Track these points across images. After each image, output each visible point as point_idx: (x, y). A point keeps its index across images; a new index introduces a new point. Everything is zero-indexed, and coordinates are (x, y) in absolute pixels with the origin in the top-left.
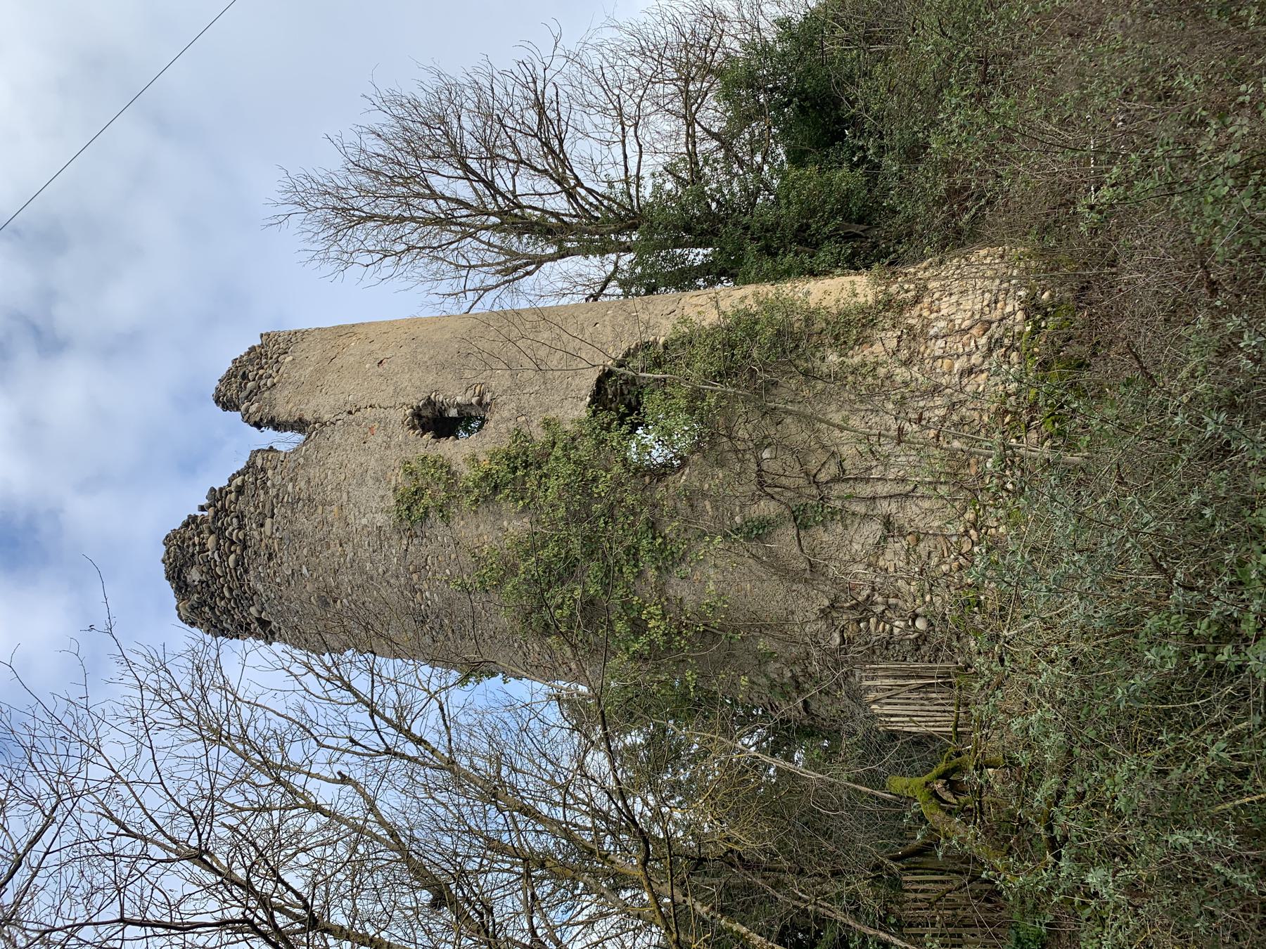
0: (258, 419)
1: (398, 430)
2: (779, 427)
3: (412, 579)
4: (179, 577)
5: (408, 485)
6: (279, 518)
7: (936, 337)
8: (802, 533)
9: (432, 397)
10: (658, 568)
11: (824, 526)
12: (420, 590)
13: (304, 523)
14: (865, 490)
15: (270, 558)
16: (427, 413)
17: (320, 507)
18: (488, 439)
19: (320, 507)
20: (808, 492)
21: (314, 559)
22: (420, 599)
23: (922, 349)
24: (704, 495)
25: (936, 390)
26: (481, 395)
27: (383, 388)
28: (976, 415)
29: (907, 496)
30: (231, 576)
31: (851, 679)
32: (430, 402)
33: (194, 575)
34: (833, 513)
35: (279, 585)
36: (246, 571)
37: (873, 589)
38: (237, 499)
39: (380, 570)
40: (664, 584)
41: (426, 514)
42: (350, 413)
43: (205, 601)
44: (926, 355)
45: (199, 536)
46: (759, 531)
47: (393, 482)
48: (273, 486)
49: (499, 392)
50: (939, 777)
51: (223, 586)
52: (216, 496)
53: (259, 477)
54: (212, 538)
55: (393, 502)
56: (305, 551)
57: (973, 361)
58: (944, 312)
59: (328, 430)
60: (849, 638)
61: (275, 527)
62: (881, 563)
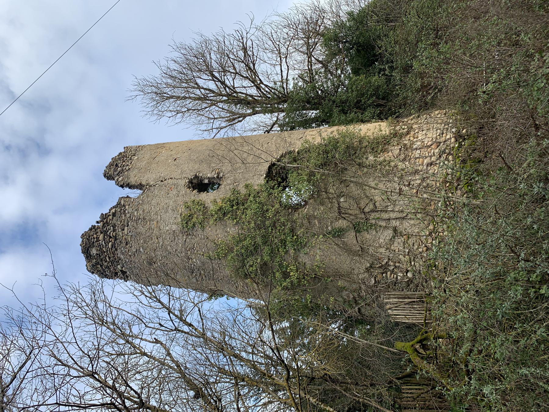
1: (183, 189)
2: (348, 188)
3: (188, 254)
4: (87, 252)
5: (187, 212)
6: (131, 227)
7: (416, 149)
8: (358, 234)
10: (294, 249)
11: (367, 231)
12: (191, 258)
14: (385, 216)
15: (126, 244)
16: (195, 181)
17: (148, 222)
18: (221, 192)
19: (148, 222)
20: (360, 216)
22: (191, 262)
23: (410, 154)
24: (315, 218)
25: (416, 172)
26: (218, 174)
27: (176, 170)
28: (434, 183)
29: (403, 218)
30: (110, 252)
31: (379, 299)
32: (196, 177)
33: (94, 251)
34: (371, 226)
35: (130, 256)
36: (116, 250)
37: (389, 259)
38: (113, 218)
40: (297, 256)
41: (194, 225)
42: (162, 181)
43: (98, 263)
44: (412, 157)
45: (96, 234)
46: (339, 233)
47: (180, 211)
48: (128, 213)
50: (418, 343)
52: (104, 217)
54: (102, 235)
55: (180, 220)
57: (432, 159)
58: (420, 138)
59: (152, 188)
60: (378, 281)
61: (129, 231)
62: (392, 248)
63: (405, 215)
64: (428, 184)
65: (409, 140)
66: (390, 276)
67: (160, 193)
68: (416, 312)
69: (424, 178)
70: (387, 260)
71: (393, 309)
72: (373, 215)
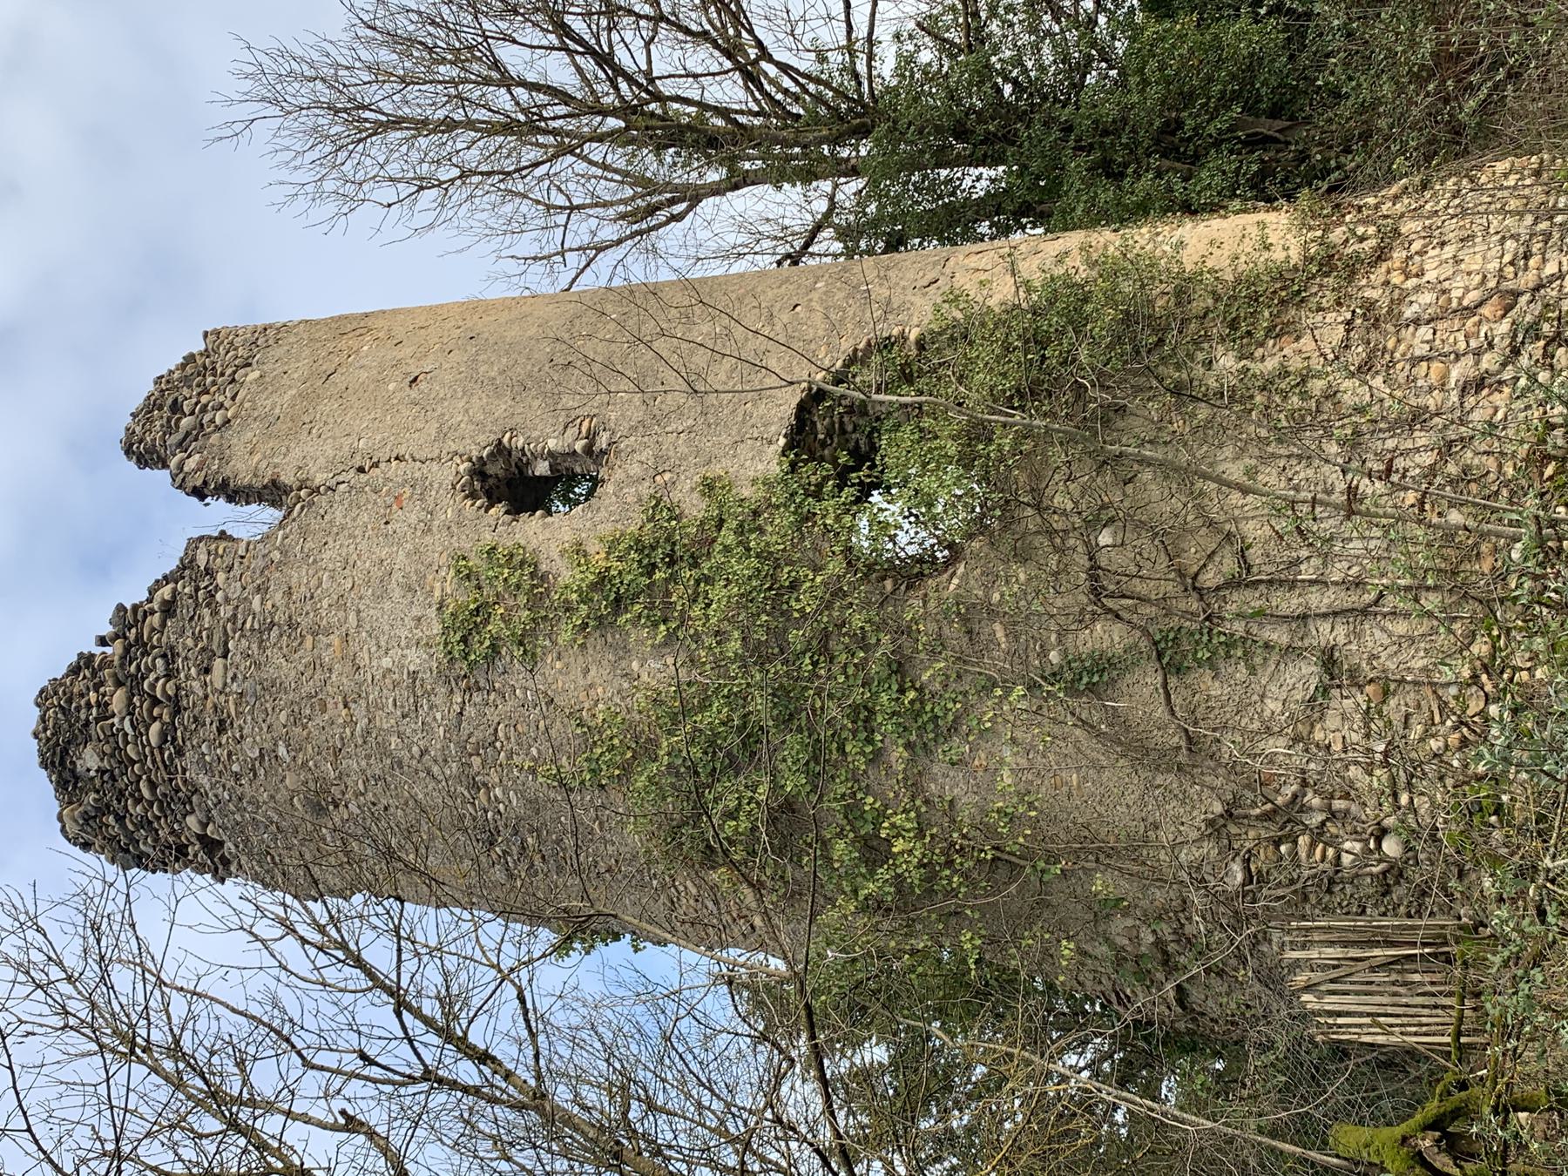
0: (199, 483)
1: (448, 500)
2: (1129, 489)
3: (470, 766)
4: (62, 763)
5: (466, 598)
6: (238, 658)
7: (1417, 322)
8: (1173, 681)
9: (505, 440)
10: (909, 746)
11: (1213, 667)
12: (485, 785)
13: (280, 667)
14: (1288, 603)
15: (221, 730)
17: (309, 639)
18: (603, 514)
19: (309, 639)
21: (299, 729)
25: (1417, 418)
26: (591, 436)
27: (419, 425)
28: (1491, 463)
29: (1364, 612)
30: (154, 761)
31: (1264, 948)
32: (500, 450)
33: (89, 760)
34: (1229, 645)
36: (180, 752)
38: (164, 625)
39: (415, 749)
42: (361, 470)
44: (1397, 355)
45: (97, 691)
47: (437, 593)
48: (227, 600)
49: (623, 429)
50: (1427, 1127)
51: (140, 778)
52: (128, 619)
53: (202, 585)
56: (283, 717)
57: (1484, 365)
59: (321, 501)
61: (230, 674)
62: (1318, 735)
63: (1369, 598)
64: (1466, 470)
65: (1387, 283)
66: (1310, 854)
67: (354, 520)
68: (1419, 1000)
69: (1450, 444)
70: (1294, 788)
71: (1323, 988)
72: (1238, 601)
